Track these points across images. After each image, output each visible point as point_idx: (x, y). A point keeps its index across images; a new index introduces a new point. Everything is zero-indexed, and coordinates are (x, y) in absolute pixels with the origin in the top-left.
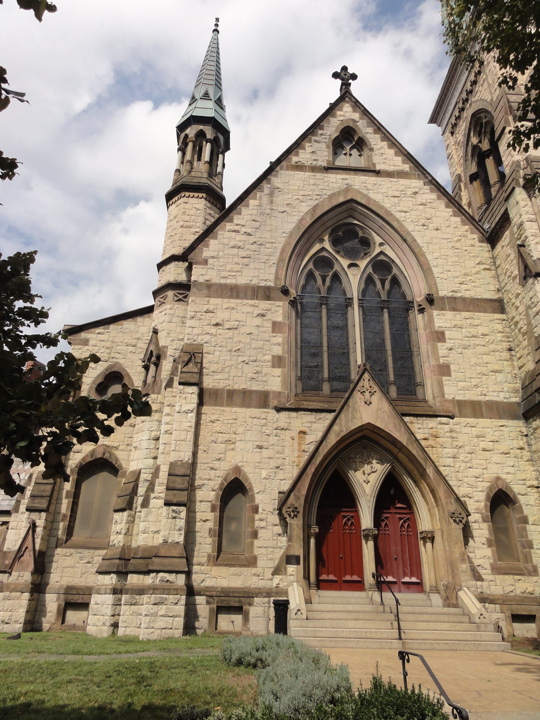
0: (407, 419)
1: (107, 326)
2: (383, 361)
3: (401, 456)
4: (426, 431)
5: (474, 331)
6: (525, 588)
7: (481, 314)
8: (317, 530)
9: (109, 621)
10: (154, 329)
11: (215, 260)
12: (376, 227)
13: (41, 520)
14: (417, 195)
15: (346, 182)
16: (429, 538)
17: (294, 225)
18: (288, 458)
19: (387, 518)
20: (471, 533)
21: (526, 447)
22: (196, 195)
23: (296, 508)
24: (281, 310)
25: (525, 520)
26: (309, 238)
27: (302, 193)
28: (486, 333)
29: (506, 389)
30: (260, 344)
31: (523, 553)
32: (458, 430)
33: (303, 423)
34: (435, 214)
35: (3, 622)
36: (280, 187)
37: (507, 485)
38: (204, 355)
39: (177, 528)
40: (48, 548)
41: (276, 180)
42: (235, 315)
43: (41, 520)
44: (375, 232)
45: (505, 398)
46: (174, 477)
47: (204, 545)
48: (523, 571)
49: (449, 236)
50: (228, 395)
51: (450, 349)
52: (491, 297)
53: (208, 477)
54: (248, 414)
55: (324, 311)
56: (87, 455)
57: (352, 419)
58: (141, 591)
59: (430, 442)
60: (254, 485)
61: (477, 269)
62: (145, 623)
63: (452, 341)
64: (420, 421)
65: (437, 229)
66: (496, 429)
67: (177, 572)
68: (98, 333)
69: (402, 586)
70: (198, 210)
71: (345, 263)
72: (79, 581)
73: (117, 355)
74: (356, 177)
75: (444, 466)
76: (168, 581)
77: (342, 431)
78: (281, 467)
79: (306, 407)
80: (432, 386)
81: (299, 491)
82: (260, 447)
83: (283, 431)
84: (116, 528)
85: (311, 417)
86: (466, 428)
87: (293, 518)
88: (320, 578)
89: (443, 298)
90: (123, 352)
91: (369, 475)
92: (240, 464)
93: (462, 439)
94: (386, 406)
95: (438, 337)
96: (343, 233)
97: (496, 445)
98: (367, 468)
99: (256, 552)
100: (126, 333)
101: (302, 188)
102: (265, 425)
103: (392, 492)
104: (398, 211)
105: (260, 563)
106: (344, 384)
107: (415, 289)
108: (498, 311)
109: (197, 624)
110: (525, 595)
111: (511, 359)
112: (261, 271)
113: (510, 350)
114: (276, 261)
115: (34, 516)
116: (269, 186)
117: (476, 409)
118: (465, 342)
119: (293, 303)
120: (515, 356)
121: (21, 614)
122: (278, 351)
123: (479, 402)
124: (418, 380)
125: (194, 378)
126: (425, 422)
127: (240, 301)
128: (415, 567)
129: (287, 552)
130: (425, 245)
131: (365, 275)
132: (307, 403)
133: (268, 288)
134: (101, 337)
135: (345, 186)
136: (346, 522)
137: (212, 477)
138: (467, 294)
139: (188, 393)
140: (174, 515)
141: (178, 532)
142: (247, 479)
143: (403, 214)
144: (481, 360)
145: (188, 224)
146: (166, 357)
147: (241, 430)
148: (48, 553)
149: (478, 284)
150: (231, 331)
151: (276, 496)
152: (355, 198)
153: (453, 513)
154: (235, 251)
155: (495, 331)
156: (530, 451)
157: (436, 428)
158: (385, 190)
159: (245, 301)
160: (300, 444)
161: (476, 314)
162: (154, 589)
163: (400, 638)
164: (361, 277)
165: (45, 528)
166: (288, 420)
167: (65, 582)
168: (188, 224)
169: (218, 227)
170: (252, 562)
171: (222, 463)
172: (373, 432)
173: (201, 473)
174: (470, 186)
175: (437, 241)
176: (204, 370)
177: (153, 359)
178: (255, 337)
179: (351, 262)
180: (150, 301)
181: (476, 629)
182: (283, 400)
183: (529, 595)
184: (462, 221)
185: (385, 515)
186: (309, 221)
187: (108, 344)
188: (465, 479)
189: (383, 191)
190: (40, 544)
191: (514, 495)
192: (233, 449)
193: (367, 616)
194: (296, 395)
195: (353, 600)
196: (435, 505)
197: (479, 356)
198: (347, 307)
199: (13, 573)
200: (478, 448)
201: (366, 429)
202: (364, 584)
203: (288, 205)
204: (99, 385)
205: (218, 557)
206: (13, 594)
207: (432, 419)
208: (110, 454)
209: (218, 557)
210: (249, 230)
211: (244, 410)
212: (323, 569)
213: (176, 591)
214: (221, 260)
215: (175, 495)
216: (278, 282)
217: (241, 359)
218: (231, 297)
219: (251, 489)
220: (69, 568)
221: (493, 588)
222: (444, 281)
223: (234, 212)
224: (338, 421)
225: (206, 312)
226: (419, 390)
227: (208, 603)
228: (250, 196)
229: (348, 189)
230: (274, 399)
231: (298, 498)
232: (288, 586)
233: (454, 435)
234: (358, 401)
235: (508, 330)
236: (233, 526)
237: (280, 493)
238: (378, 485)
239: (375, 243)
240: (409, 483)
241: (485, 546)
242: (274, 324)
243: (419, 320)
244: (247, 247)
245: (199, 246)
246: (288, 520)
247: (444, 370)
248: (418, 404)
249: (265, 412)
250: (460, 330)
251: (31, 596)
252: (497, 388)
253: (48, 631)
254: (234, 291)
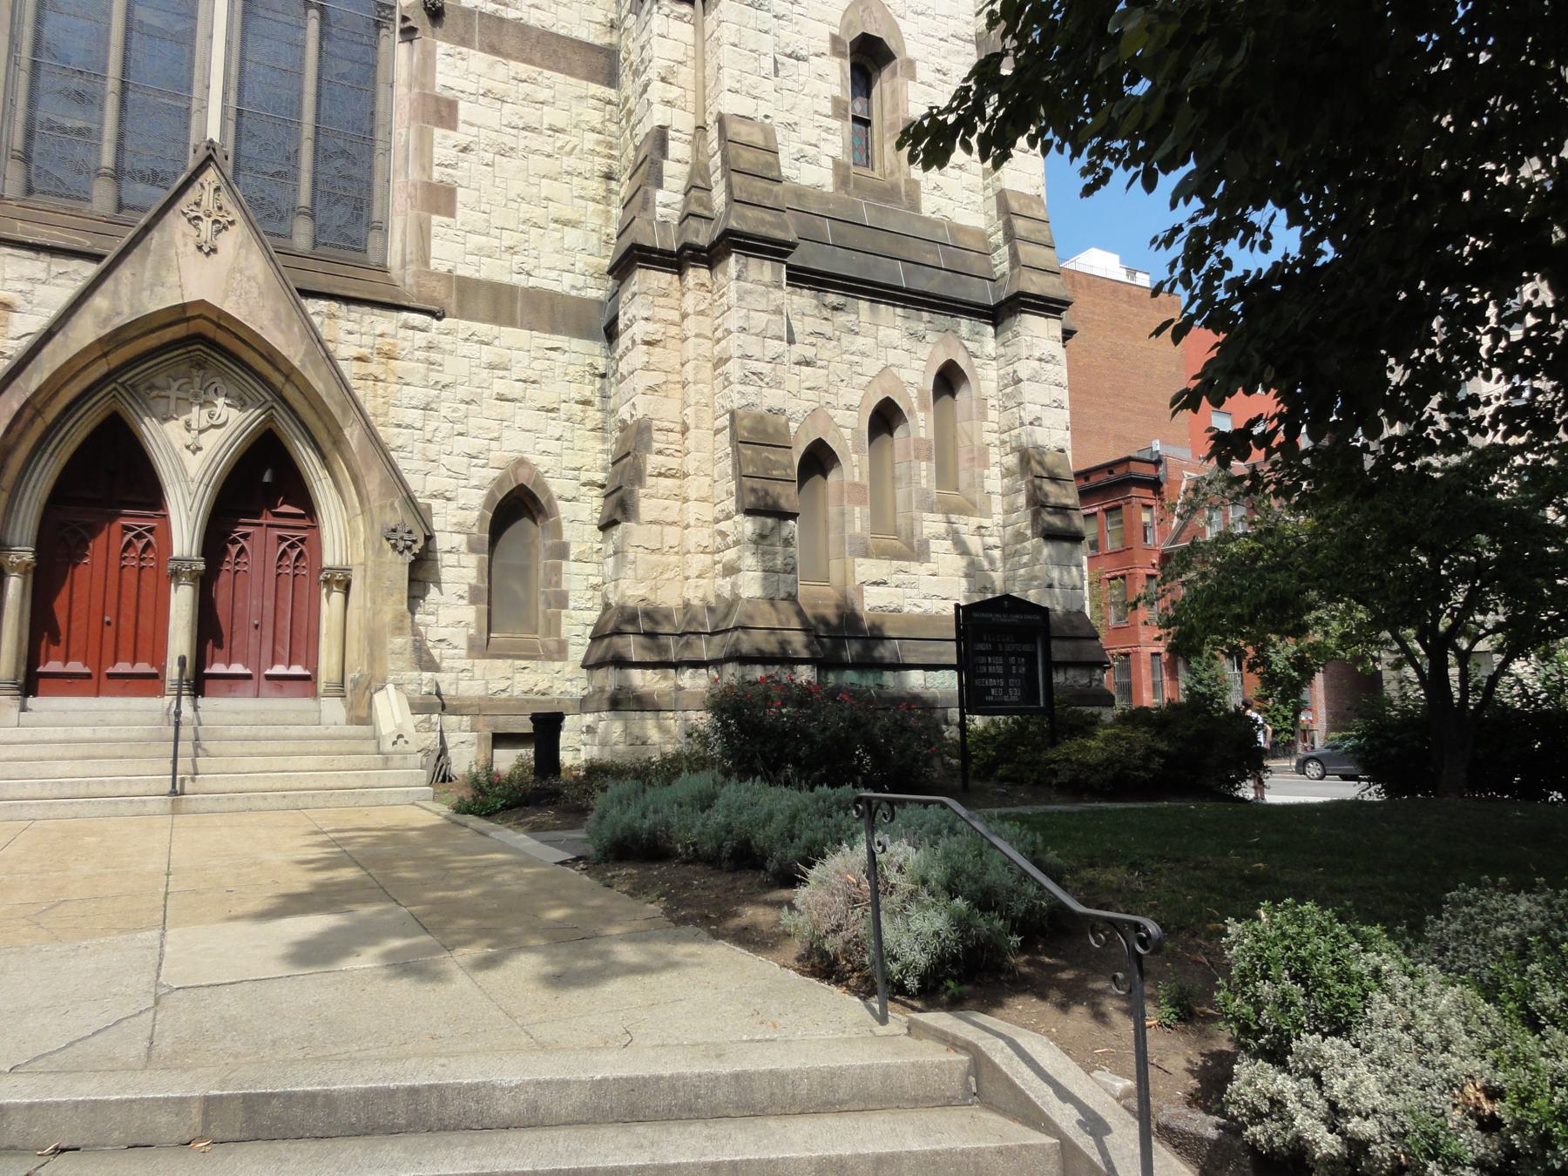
0: (311, 306)
2: (292, 150)
3: (290, 392)
4: (367, 340)
5: (531, 115)
6: (532, 682)
7: (559, 77)
19: (245, 536)
20: (437, 574)
21: (597, 400)
25: (562, 551)
28: (560, 125)
32: (448, 347)
33: (5, 280)
37: (539, 479)
45: (573, 287)
48: (536, 649)
51: (465, 150)
52: (591, 40)
57: (153, 285)
59: (372, 368)
63: (474, 130)
64: (354, 316)
66: (539, 354)
75: (399, 426)
77: (118, 314)
80: (404, 233)
85: (36, 266)
86: (465, 344)
89: (469, 13)
91: (201, 432)
93: (453, 368)
94: (257, 264)
95: (438, 112)
97: (531, 390)
98: (198, 416)
103: (267, 478)
106: (152, 195)
108: (600, 78)
111: (606, 200)
113: (609, 177)
117: (501, 303)
118: (506, 139)
120: (617, 193)
123: (512, 290)
124: (376, 216)
126: (367, 319)
128: (303, 642)
132: (29, 226)
155: (583, 126)
156: (602, 410)
157: (394, 337)
161: (547, 73)
172: (219, 326)
181: (380, 764)
185: (242, 530)
188: (444, 459)
191: (550, 500)
195: (119, 717)
196: (359, 511)
197: (532, 180)
200: (487, 393)
202: (164, 681)
212: (53, 649)
221: (463, 685)
224: (109, 284)
226: (374, 240)
233: (434, 356)
234: (178, 239)
235: (614, 128)
238: (225, 459)
240: (307, 459)
243: (401, 58)
247: (441, 198)
250: (498, 104)
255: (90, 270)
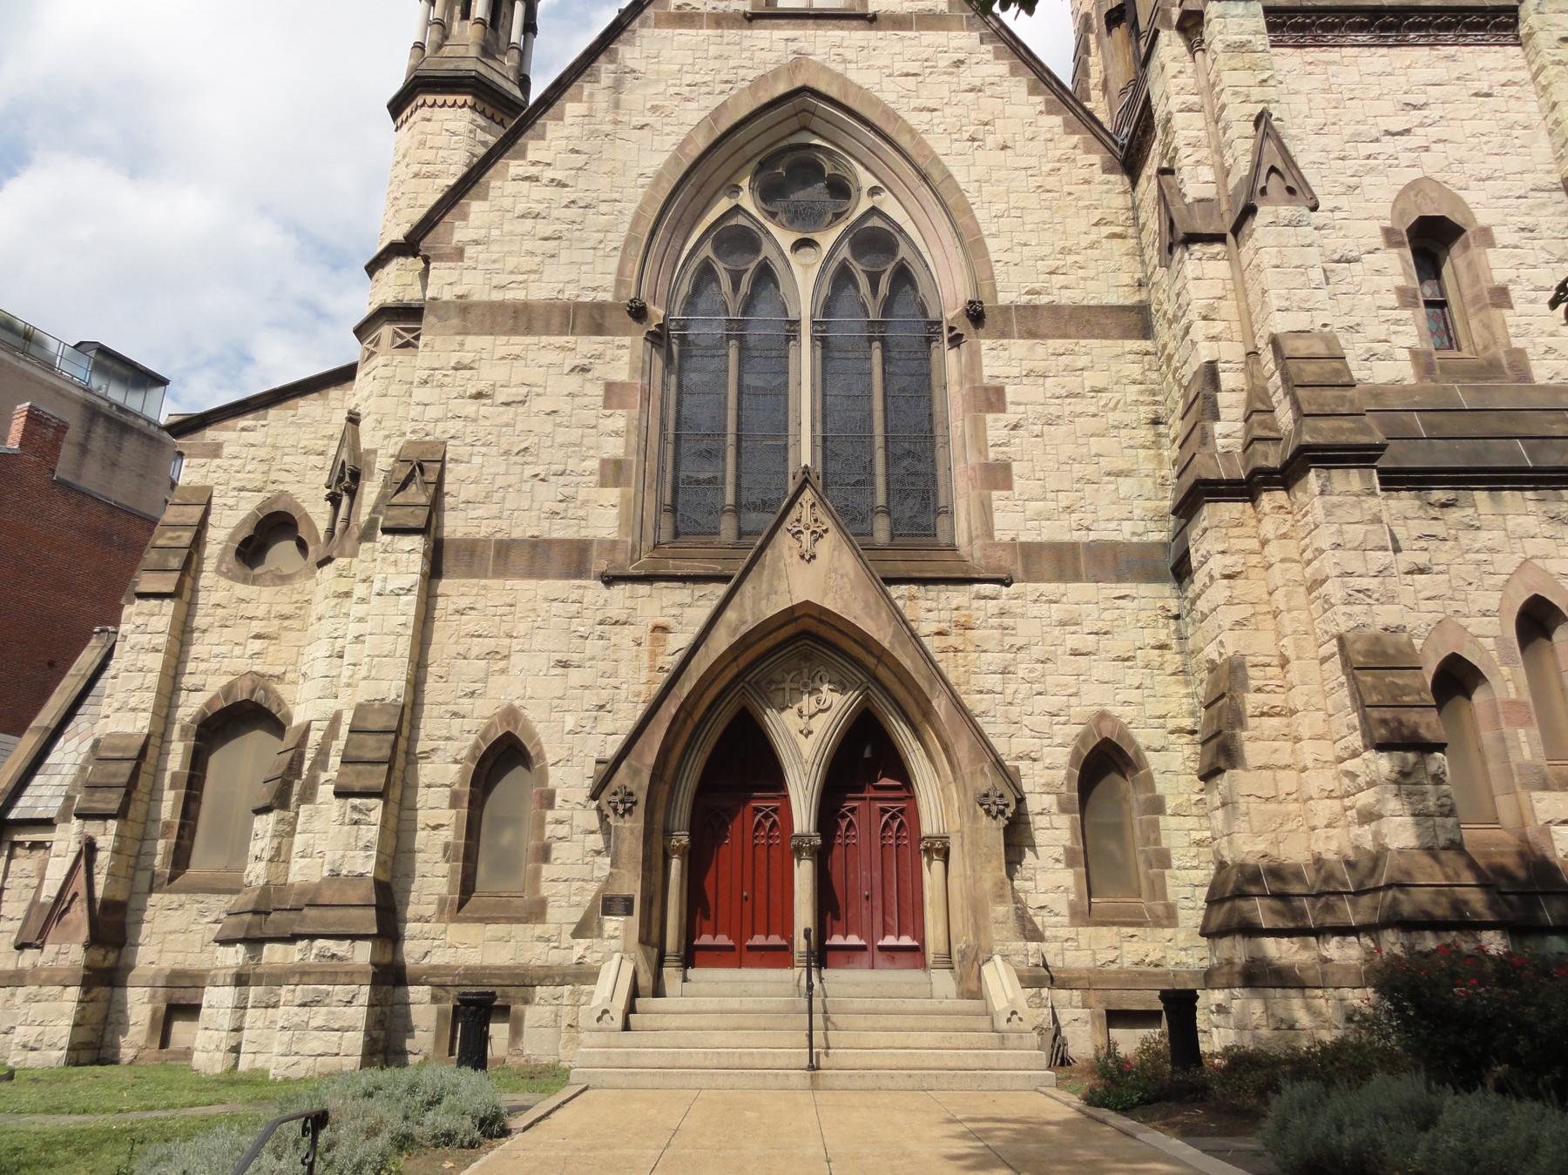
0: (895, 591)
1: (262, 412)
3: (882, 672)
5: (1072, 382)
6: (1142, 952)
8: (685, 840)
9: (227, 1040)
10: (350, 412)
11: (480, 248)
12: (862, 151)
13: (106, 836)
14: (963, 68)
15: (793, 46)
16: (938, 851)
17: (666, 156)
18: (624, 686)
19: (852, 810)
20: (1031, 837)
21: (1174, 643)
22: (450, 99)
23: (631, 794)
24: (625, 355)
25: (1157, 806)
26: (702, 186)
27: (688, 79)
28: (1100, 385)
29: (1137, 512)
30: (574, 434)
31: (1147, 876)
34: (1003, 110)
35: (24, 1046)
36: (636, 67)
37: (1123, 731)
38: (448, 466)
39: (361, 844)
40: (132, 893)
41: (628, 53)
42: (520, 372)
43: (106, 836)
44: (862, 164)
45: (1134, 534)
46: (362, 736)
47: (432, 878)
48: (1143, 916)
49: (1032, 162)
50: (498, 553)
51: (1015, 427)
53: (445, 733)
54: (541, 592)
55: (877, 354)
56: (216, 697)
57: (769, 594)
58: (278, 978)
59: (951, 640)
60: (546, 748)
61: (1092, 237)
62: (281, 1044)
64: (932, 595)
65: (1004, 148)
67: (354, 937)
68: (243, 429)
69: (879, 956)
70: (454, 134)
71: (785, 238)
72: (193, 961)
73: (283, 476)
74: (819, 32)
76: (333, 956)
78: (608, 707)
79: (672, 571)
80: (968, 513)
81: (640, 757)
82: (565, 665)
83: (618, 628)
84: (255, 847)
85: (682, 593)
86: (1035, 606)
87: (622, 816)
88: (696, 942)
90: (295, 467)
91: (811, 717)
92: (517, 703)
93: (1025, 631)
94: (848, 562)
95: (988, 399)
96: (788, 171)
98: (808, 703)
99: (546, 890)
100: (305, 425)
101: (689, 68)
102: (578, 615)
103: (867, 754)
104: (915, 109)
105: (553, 913)
106: (760, 520)
107: (946, 292)
109: (409, 1044)
110: (1143, 968)
112: (584, 268)
114: (620, 244)
115: (93, 828)
116: (612, 67)
117: (1064, 561)
118: (1051, 410)
119: (658, 338)
120: (1167, 436)
121: (62, 1030)
122: (615, 448)
123: (1074, 546)
124: (942, 502)
125: (416, 516)
126: (943, 596)
127: (535, 339)
128: (910, 914)
129: (606, 889)
130: (973, 187)
131: (834, 265)
133: (600, 307)
134: (249, 437)
135: (791, 57)
136: (759, 822)
137: (455, 732)
138: (1065, 298)
139: (403, 551)
140: (356, 816)
141: (363, 853)
142: (532, 735)
143: (926, 116)
144: (1084, 450)
145: (431, 168)
146: (372, 473)
147: (522, 627)
148: (133, 904)
149: (1092, 273)
150: (511, 409)
151: (590, 769)
152: (812, 84)
153: (986, 796)
154: (529, 222)
155: (1124, 381)
157: (968, 608)
158: (887, 62)
159: (545, 339)
160: (653, 655)
161: (1083, 342)
162: (302, 974)
163: (812, 1068)
164: (823, 270)
165: (116, 852)
166: (629, 603)
167: (168, 962)
168: (431, 168)
169: (491, 171)
170: (536, 912)
171: (479, 702)
172: (821, 621)
173: (431, 725)
174: (1106, 40)
175: (1003, 174)
176: (447, 499)
177: (346, 482)
178: (565, 421)
179: (800, 236)
180: (348, 350)
182: (621, 557)
183: (1152, 969)
184: (1067, 124)
186: (701, 143)
187: (263, 453)
188: (1026, 720)
189: (880, 63)
190: (106, 886)
191: (1138, 752)
192: (503, 671)
193: (763, 1021)
194: (657, 545)
196: (951, 778)
197: (1080, 441)
198: (788, 339)
199: (47, 947)
200: (1060, 650)
201: (805, 615)
203: (654, 109)
204: (246, 543)
205: (461, 905)
206: (46, 989)
207: (961, 588)
208: (266, 690)
209: (461, 905)
210: (559, 175)
211: (531, 584)
212: (706, 923)
213: (350, 977)
214: (494, 248)
215: (359, 774)
216: (623, 292)
217: (529, 471)
218: (514, 331)
219: (541, 756)
220: (174, 933)
222: (1012, 268)
223: (530, 133)
224: (736, 599)
225: (455, 369)
226: (942, 522)
227: (435, 999)
228: (566, 95)
229: (799, 62)
230: (600, 556)
231: (636, 772)
232: (603, 960)
233: (1007, 621)
234: (786, 553)
235: (1154, 376)
236: (507, 837)
237: (598, 762)
239: (859, 190)
241: (1062, 865)
242: (610, 387)
243: (951, 362)
244: (555, 213)
245: (446, 219)
246: (611, 820)
247: (998, 475)
248: (934, 555)
249: (579, 587)
250: (1041, 380)
251: (86, 993)
252: (1118, 511)
253: (131, 1063)
254: (521, 318)
255: (721, 589)
